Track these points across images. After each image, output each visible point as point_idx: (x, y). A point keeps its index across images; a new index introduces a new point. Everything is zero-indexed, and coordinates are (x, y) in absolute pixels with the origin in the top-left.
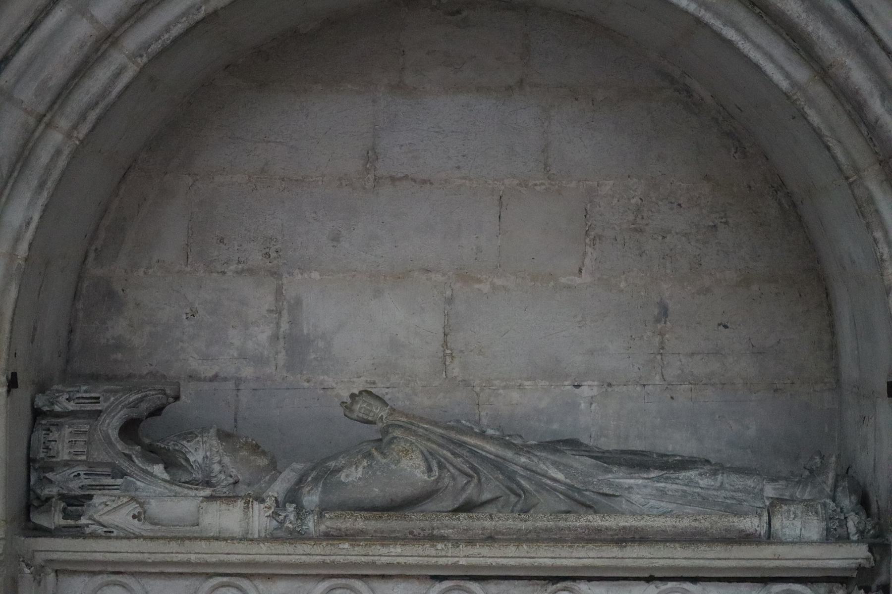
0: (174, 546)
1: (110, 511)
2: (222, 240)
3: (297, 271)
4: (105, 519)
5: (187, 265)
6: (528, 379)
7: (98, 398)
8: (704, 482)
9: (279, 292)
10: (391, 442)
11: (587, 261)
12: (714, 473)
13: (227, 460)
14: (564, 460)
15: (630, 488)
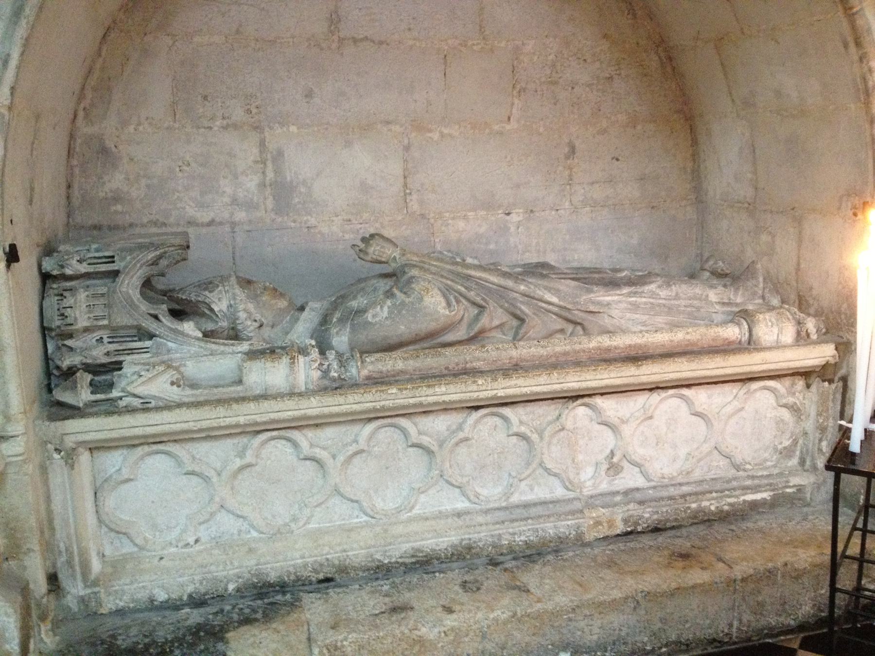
0: (221, 411)
1: (140, 379)
3: (277, 125)
4: (139, 391)
5: (175, 122)
6: (470, 211)
7: (113, 257)
8: (663, 293)
9: (262, 144)
11: (514, 111)
13: (251, 307)
14: (551, 285)
15: (608, 304)
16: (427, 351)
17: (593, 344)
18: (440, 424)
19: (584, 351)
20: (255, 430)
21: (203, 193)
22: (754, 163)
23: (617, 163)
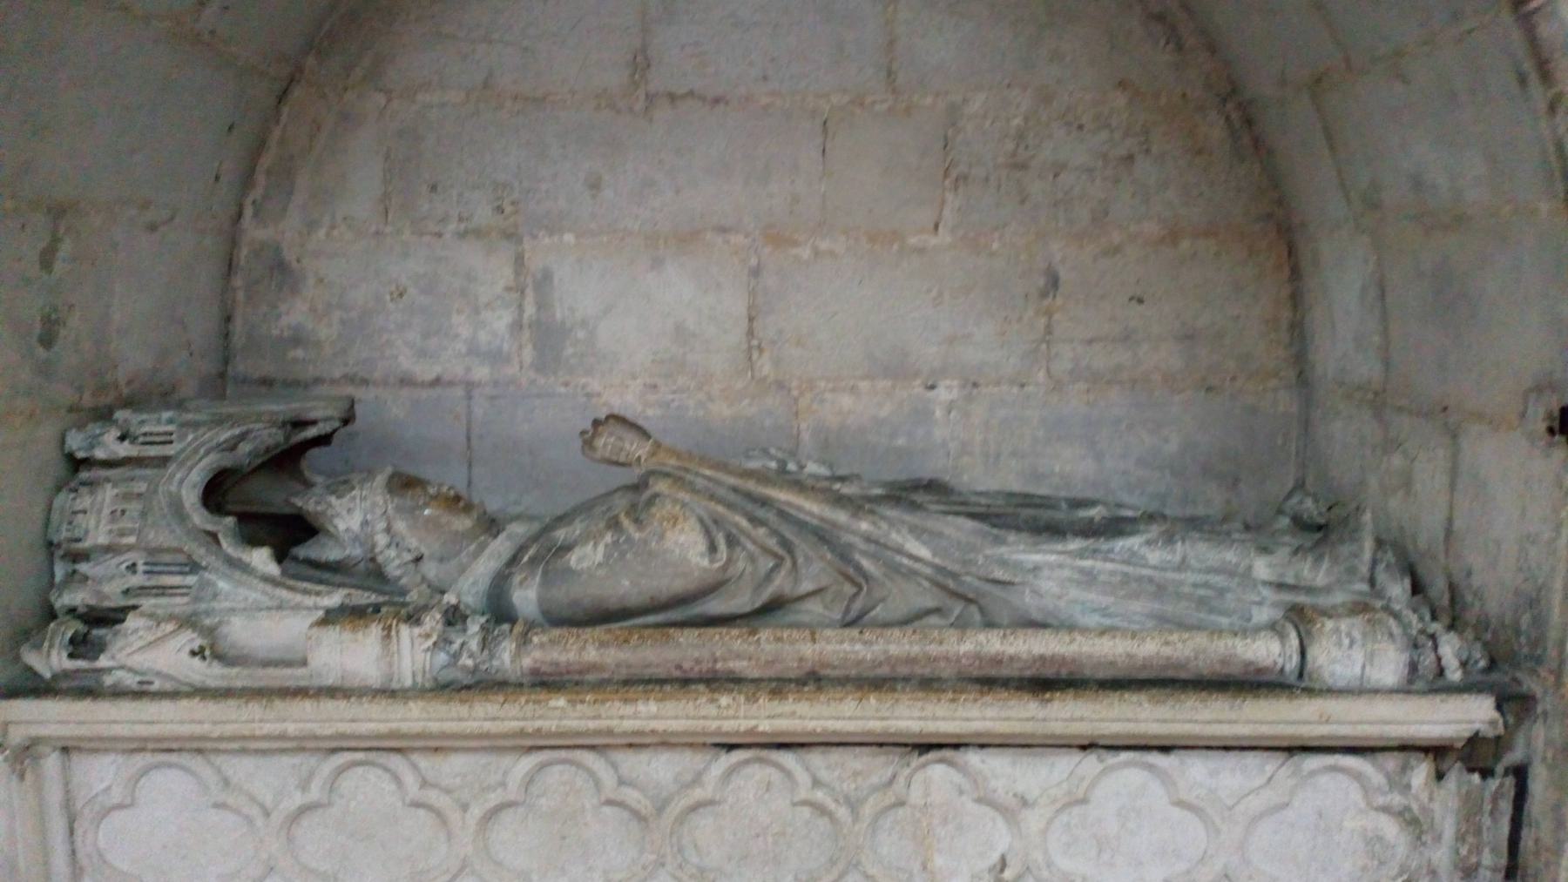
0: (255, 709)
2: (434, 188)
5: (386, 223)
6: (863, 378)
8: (1155, 556)
9: (519, 261)
10: (651, 502)
11: (947, 212)
12: (1169, 539)
13: (400, 526)
15: (1036, 569)
16: (647, 632)
17: (967, 647)
18: (661, 768)
19: (947, 659)
20: (335, 746)
21: (426, 335)
22: (1385, 317)
23: (1140, 308)
